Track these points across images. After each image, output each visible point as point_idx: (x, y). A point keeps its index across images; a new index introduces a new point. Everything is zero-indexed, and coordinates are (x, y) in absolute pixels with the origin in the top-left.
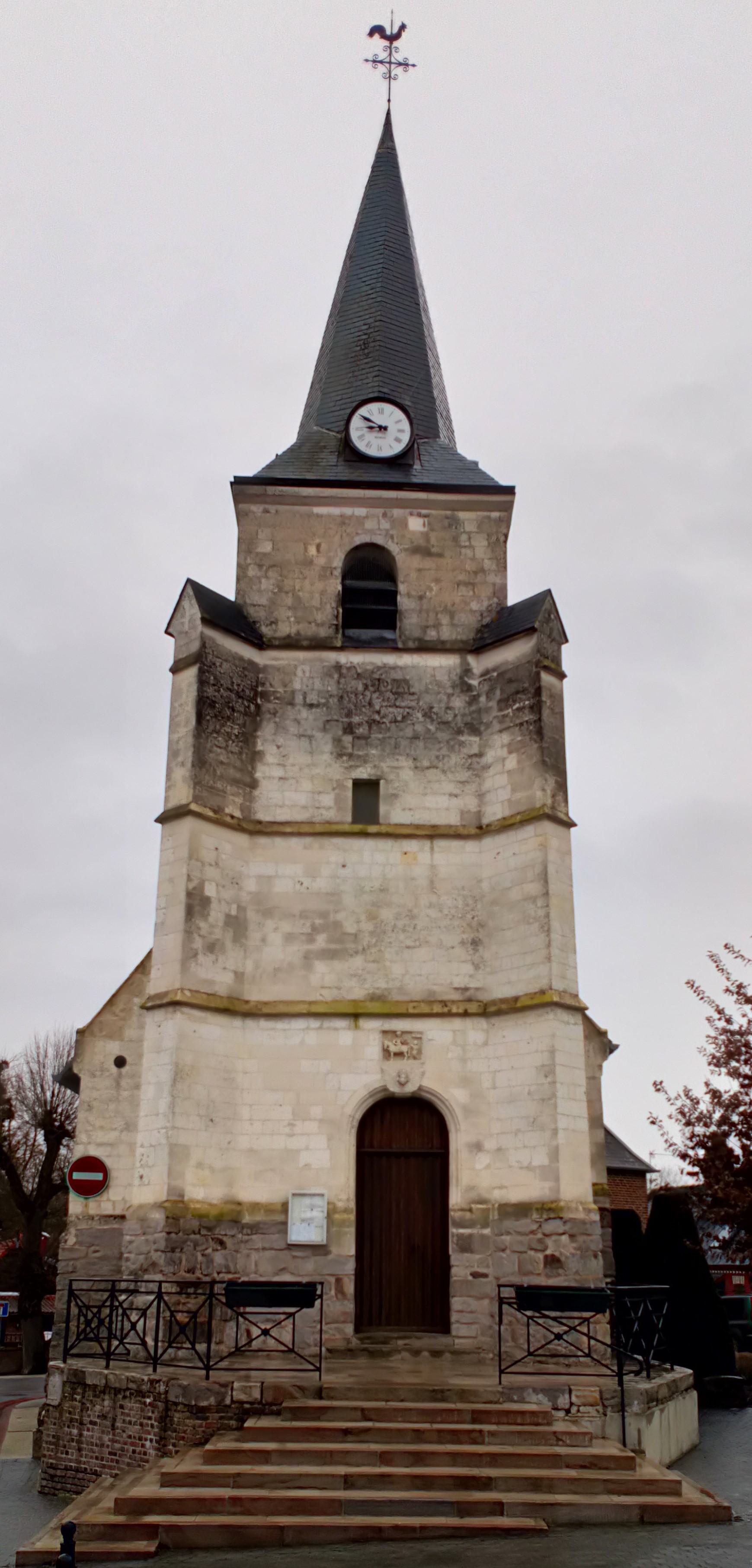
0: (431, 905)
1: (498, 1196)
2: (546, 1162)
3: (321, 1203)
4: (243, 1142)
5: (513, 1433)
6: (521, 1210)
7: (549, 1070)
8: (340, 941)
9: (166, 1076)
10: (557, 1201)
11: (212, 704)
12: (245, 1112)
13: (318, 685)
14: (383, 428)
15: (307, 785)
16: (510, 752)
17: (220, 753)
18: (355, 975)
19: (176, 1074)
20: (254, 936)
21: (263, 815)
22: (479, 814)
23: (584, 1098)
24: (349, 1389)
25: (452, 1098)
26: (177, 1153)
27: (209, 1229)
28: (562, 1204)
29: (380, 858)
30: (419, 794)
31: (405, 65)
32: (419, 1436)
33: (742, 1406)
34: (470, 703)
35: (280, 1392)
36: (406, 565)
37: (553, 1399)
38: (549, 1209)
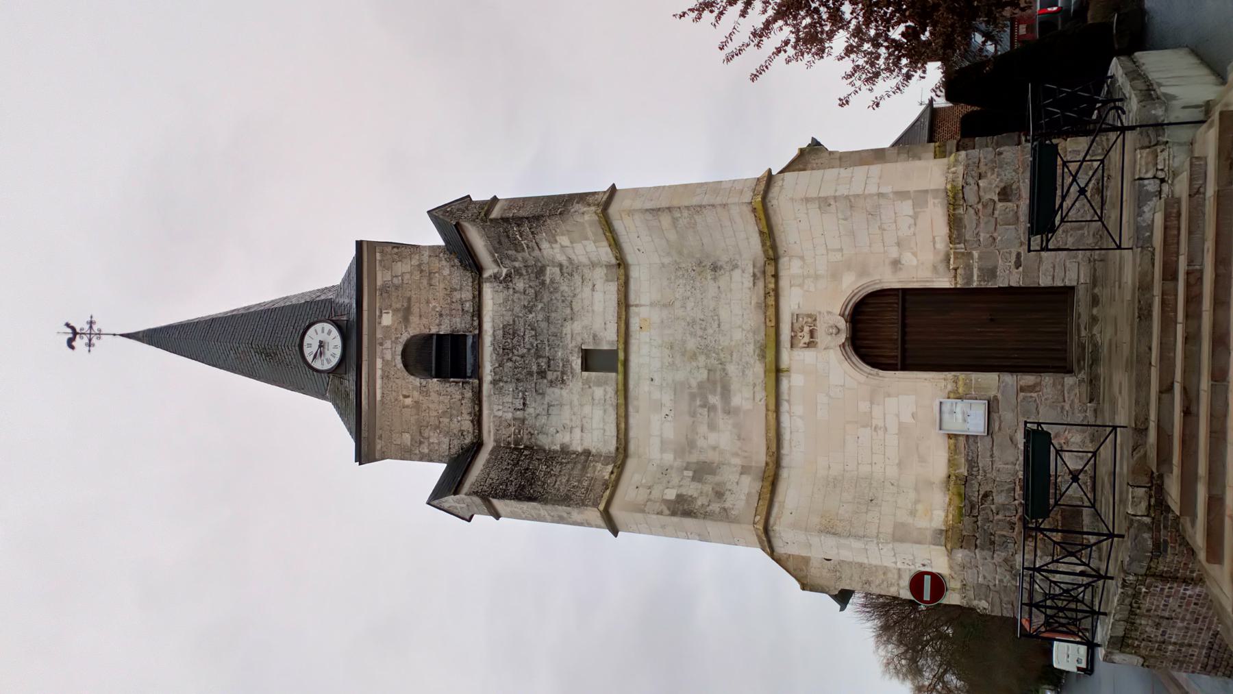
0: (684, 306)
1: (942, 245)
2: (910, 202)
3: (948, 404)
4: (892, 472)
5: (1190, 240)
6: (955, 223)
7: (824, 203)
8: (714, 383)
9: (831, 541)
10: (946, 191)
11: (522, 487)
12: (865, 469)
13: (509, 399)
14: (321, 345)
15: (587, 410)
16: (556, 241)
17: (561, 481)
18: (743, 372)
19: (828, 532)
20: (712, 456)
21: (612, 446)
22: (608, 266)
23: (850, 170)
24: (1137, 402)
25: (851, 286)
26: (901, 535)
27: (972, 507)
28: (949, 187)
29: (645, 350)
30: (592, 317)
31: (91, 323)
32: (1192, 338)
33: (1142, 12)
34: (521, 275)
35: (1140, 468)
36: (417, 327)
37: (1148, 196)
38: (955, 200)
